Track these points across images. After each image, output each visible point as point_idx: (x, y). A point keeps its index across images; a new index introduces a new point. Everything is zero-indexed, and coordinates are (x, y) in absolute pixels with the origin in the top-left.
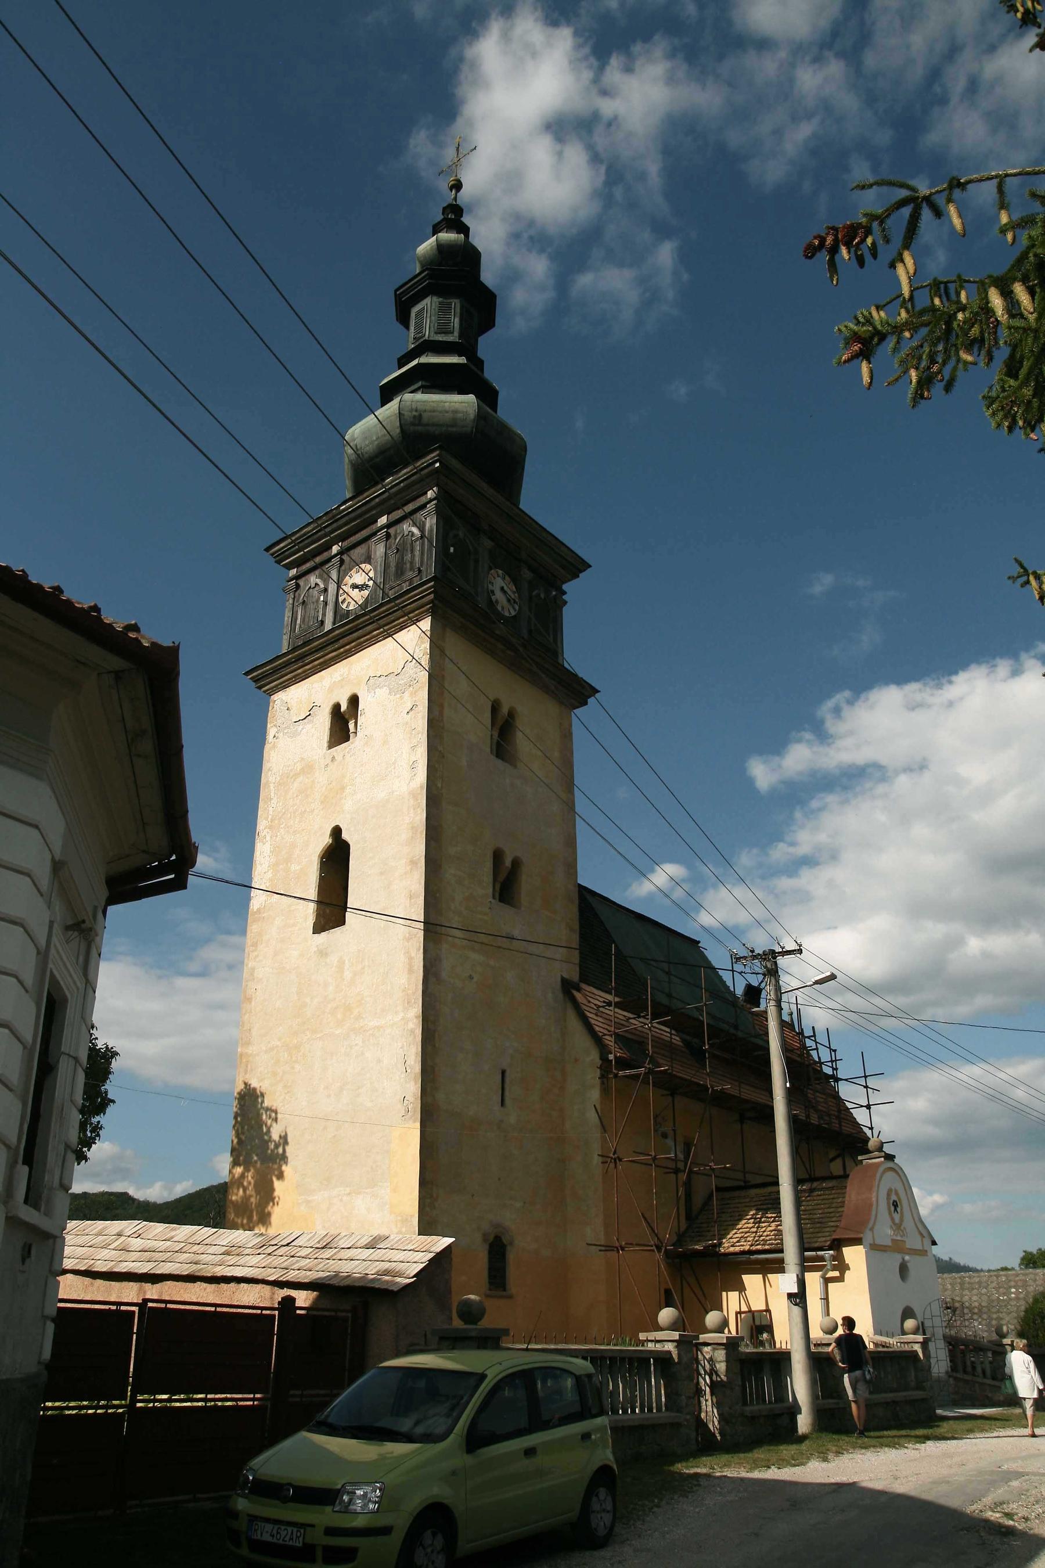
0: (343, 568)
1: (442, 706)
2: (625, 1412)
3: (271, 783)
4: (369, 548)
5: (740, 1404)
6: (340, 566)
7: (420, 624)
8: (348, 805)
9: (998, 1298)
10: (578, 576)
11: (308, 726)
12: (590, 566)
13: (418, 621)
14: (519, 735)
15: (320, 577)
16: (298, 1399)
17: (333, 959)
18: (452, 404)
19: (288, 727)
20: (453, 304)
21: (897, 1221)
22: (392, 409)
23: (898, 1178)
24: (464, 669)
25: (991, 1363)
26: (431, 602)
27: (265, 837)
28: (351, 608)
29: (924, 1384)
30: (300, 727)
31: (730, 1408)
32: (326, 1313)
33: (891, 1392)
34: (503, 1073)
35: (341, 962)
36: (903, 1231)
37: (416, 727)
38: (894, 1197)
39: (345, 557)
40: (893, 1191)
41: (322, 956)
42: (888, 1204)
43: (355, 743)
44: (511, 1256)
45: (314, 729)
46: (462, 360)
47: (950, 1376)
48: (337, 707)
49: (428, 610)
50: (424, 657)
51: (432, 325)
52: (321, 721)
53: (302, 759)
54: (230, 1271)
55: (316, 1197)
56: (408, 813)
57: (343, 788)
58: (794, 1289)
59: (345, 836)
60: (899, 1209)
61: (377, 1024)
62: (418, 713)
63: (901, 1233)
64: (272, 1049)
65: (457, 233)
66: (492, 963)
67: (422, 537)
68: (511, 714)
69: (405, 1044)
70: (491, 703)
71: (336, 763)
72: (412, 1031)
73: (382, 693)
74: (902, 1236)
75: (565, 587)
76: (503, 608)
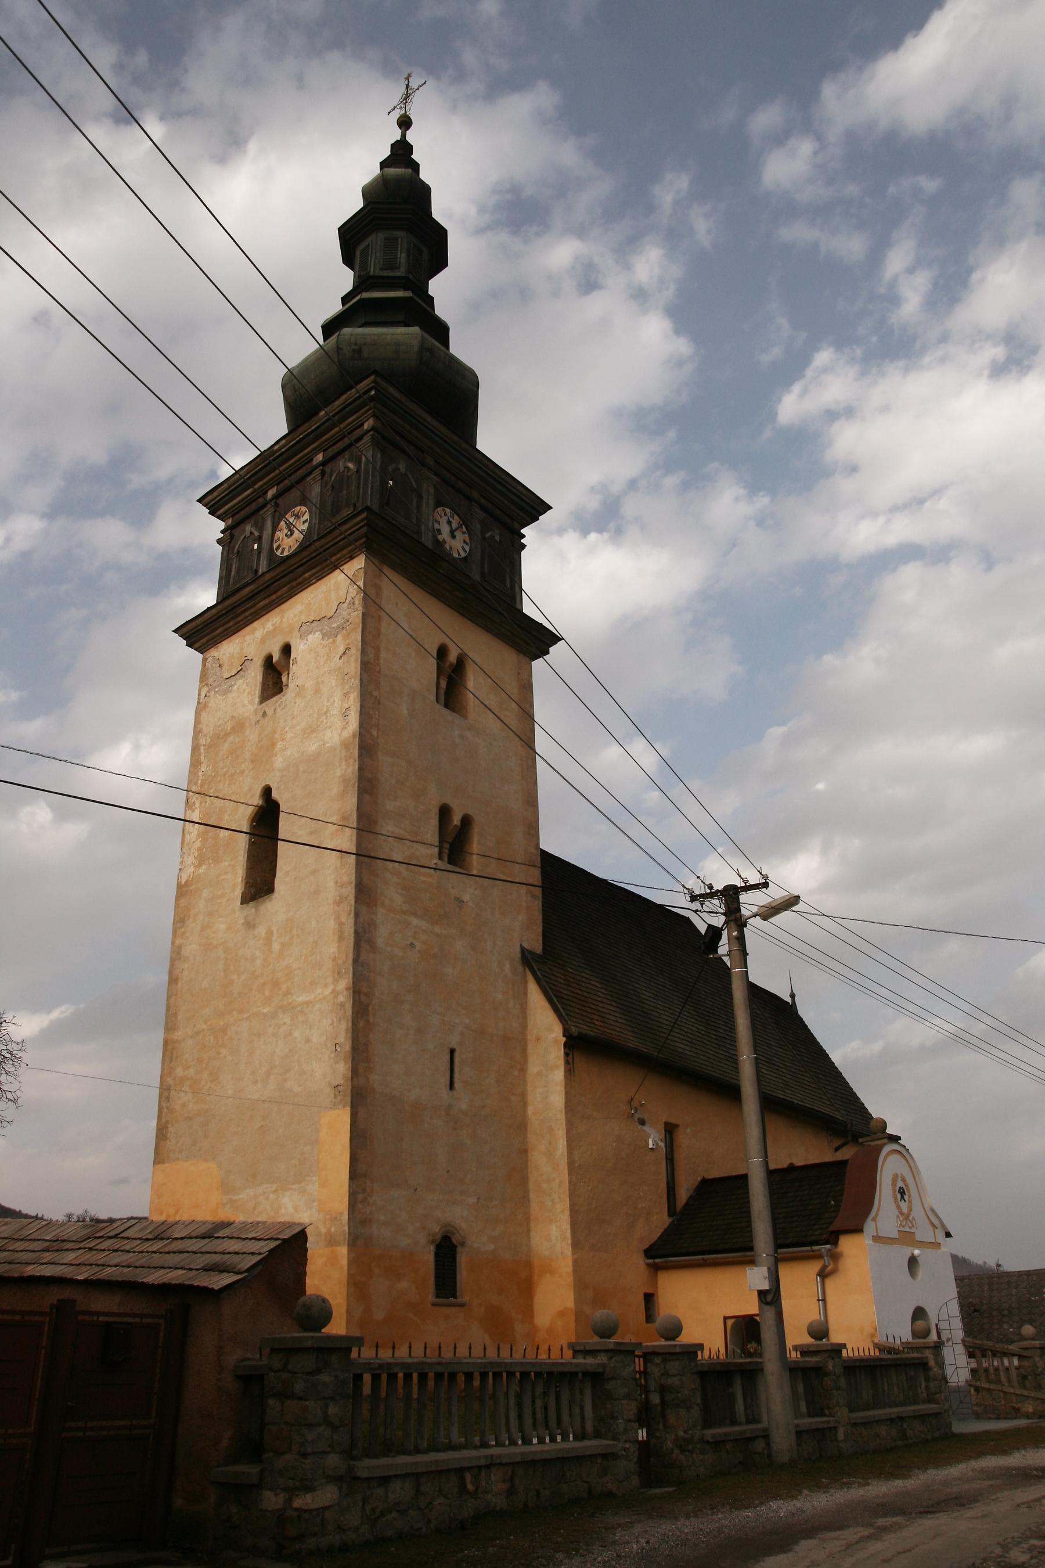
1: (377, 649)
2: (541, 1441)
5: (699, 1428)
8: (279, 762)
9: (1029, 1298)
10: (538, 519)
11: (240, 682)
12: (551, 508)
15: (256, 525)
16: (80, 1434)
17: (261, 930)
18: (395, 336)
19: (220, 685)
20: (400, 240)
21: (905, 1210)
22: (330, 344)
23: (904, 1162)
25: (1017, 1368)
26: (365, 535)
27: (194, 803)
28: (286, 554)
29: (938, 1396)
30: (232, 681)
31: (685, 1432)
32: (130, 1320)
33: (896, 1406)
34: (452, 1052)
35: (270, 933)
36: (911, 1223)
37: (349, 671)
38: (900, 1184)
40: (900, 1178)
41: (249, 928)
42: (894, 1191)
43: (289, 694)
44: (463, 1259)
45: (245, 685)
46: (407, 294)
47: (970, 1385)
48: (269, 659)
52: (253, 675)
53: (233, 717)
54: (41, 1270)
55: (241, 1196)
56: (340, 766)
57: (273, 745)
58: (765, 1286)
59: (275, 795)
60: (906, 1197)
61: (306, 999)
62: (351, 656)
63: (910, 1225)
64: (198, 1033)
65: (405, 168)
66: (437, 929)
67: (358, 471)
69: (335, 1019)
71: (267, 718)
72: (342, 1005)
73: (314, 638)
74: (910, 1228)
75: (522, 531)
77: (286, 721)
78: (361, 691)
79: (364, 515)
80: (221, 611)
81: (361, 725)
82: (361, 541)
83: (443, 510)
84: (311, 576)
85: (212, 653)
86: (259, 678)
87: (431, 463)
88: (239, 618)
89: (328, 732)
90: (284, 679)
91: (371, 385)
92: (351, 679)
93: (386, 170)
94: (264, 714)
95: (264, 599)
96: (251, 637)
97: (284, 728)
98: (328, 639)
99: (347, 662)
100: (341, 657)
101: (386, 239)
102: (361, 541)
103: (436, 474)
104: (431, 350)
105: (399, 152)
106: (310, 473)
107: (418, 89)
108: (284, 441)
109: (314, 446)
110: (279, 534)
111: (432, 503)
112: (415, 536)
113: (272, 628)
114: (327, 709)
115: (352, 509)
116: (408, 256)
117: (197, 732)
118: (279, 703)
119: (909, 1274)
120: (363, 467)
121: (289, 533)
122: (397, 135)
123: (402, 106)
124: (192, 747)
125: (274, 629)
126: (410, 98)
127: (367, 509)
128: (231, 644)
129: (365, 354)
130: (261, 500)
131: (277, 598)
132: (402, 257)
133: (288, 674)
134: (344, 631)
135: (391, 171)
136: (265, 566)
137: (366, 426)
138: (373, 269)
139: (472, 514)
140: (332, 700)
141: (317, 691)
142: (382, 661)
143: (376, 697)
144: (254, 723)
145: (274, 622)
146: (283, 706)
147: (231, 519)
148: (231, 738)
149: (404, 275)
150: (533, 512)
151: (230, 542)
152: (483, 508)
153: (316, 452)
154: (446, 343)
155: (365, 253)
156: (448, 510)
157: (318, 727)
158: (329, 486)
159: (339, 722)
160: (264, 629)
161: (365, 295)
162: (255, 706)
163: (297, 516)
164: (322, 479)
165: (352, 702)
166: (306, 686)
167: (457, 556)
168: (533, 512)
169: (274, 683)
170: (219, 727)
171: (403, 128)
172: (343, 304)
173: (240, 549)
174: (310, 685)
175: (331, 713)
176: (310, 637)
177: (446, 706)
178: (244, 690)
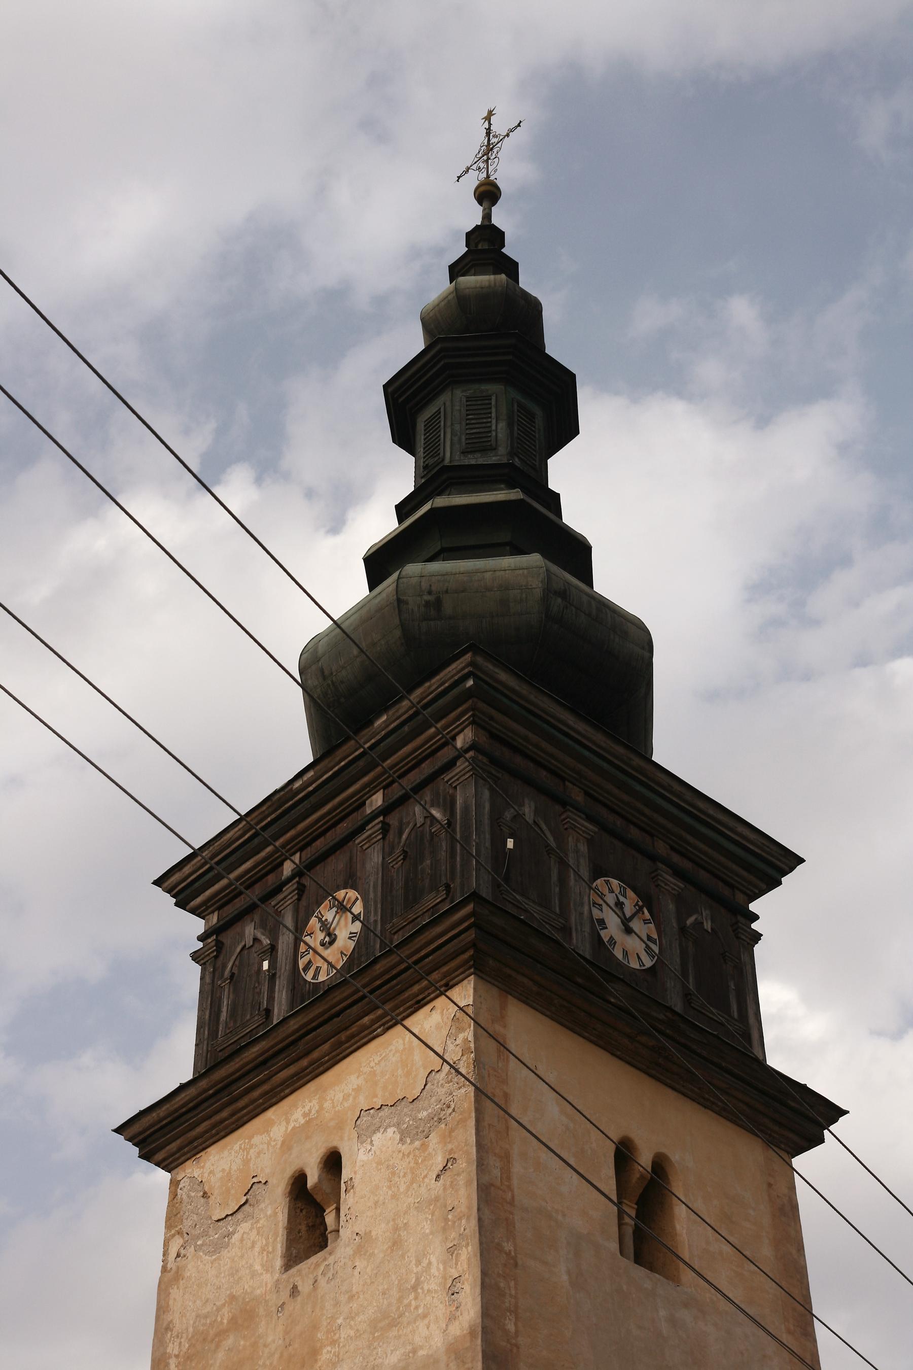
0: (304, 903)
1: (506, 1158)
3: (170, 1357)
4: (351, 859)
6: (299, 899)
7: (454, 993)
11: (245, 1226)
12: (801, 861)
13: (449, 986)
14: (680, 1212)
15: (263, 925)
18: (498, 573)
19: (205, 1234)
20: (494, 398)
22: (384, 595)
24: (551, 1078)
26: (473, 945)
28: (322, 978)
39: (306, 881)
45: (255, 1232)
46: (515, 494)
48: (299, 1179)
49: (467, 961)
50: (465, 1058)
51: (456, 439)
52: (269, 1212)
53: (232, 1298)
57: (314, 1353)
62: (458, 1174)
65: (494, 274)
67: (449, 824)
68: (660, 1166)
70: (612, 1148)
71: (299, 1298)
75: (753, 907)
76: (626, 953)
77: (337, 1304)
78: (481, 1243)
79: (470, 908)
80: (205, 1091)
81: (485, 1312)
82: (466, 956)
83: (607, 882)
84: (373, 1022)
85: (188, 1171)
86: (282, 1218)
87: (578, 796)
88: (241, 1103)
89: (421, 1325)
90: (330, 1219)
91: (466, 671)
92: (460, 1219)
94: (294, 1291)
95: (287, 1066)
96: (265, 1137)
97: (333, 1318)
98: (412, 1142)
99: (451, 1185)
100: (438, 1176)
101: (468, 399)
102: (466, 956)
103: (589, 818)
104: (564, 594)
105: (480, 247)
106: (361, 829)
107: (508, 135)
108: (311, 774)
109: (366, 779)
111: (585, 873)
112: (558, 936)
113: (302, 1121)
114: (417, 1279)
115: (443, 894)
116: (510, 425)
117: (162, 1330)
118: (322, 1268)
120: (458, 811)
121: (327, 939)
122: (473, 216)
123: (482, 165)
124: (153, 1361)
125: (308, 1123)
126: (495, 150)
127: (475, 896)
128: (226, 1153)
129: (448, 607)
130: (271, 878)
131: (311, 1064)
132: (500, 430)
133: (338, 1210)
134: (443, 1126)
135: (469, 281)
136: (284, 1002)
137: (459, 743)
138: (449, 455)
139: (657, 886)
140: (425, 1263)
141: (396, 1244)
142: (515, 1182)
143: (508, 1254)
144: (274, 1309)
145: (307, 1109)
146: (330, 1275)
147: (216, 914)
148: (229, 1342)
149: (505, 461)
150: (771, 871)
151: (216, 957)
152: (678, 873)
153: (370, 790)
154: (586, 575)
155: (433, 424)
156: (615, 882)
157: (400, 1316)
158: (398, 851)
159: (441, 1306)
160: (288, 1122)
161: (441, 501)
162: (277, 1276)
163: (342, 908)
164: (383, 838)
165: (465, 1266)
166: (374, 1233)
167: (637, 967)
168: (771, 871)
169: (308, 1225)
170: (206, 1317)
171: (485, 204)
172: (401, 519)
173: (235, 971)
174: (380, 1231)
175: (426, 1287)
176: (377, 1138)
177: (639, 1259)
178: (254, 1244)
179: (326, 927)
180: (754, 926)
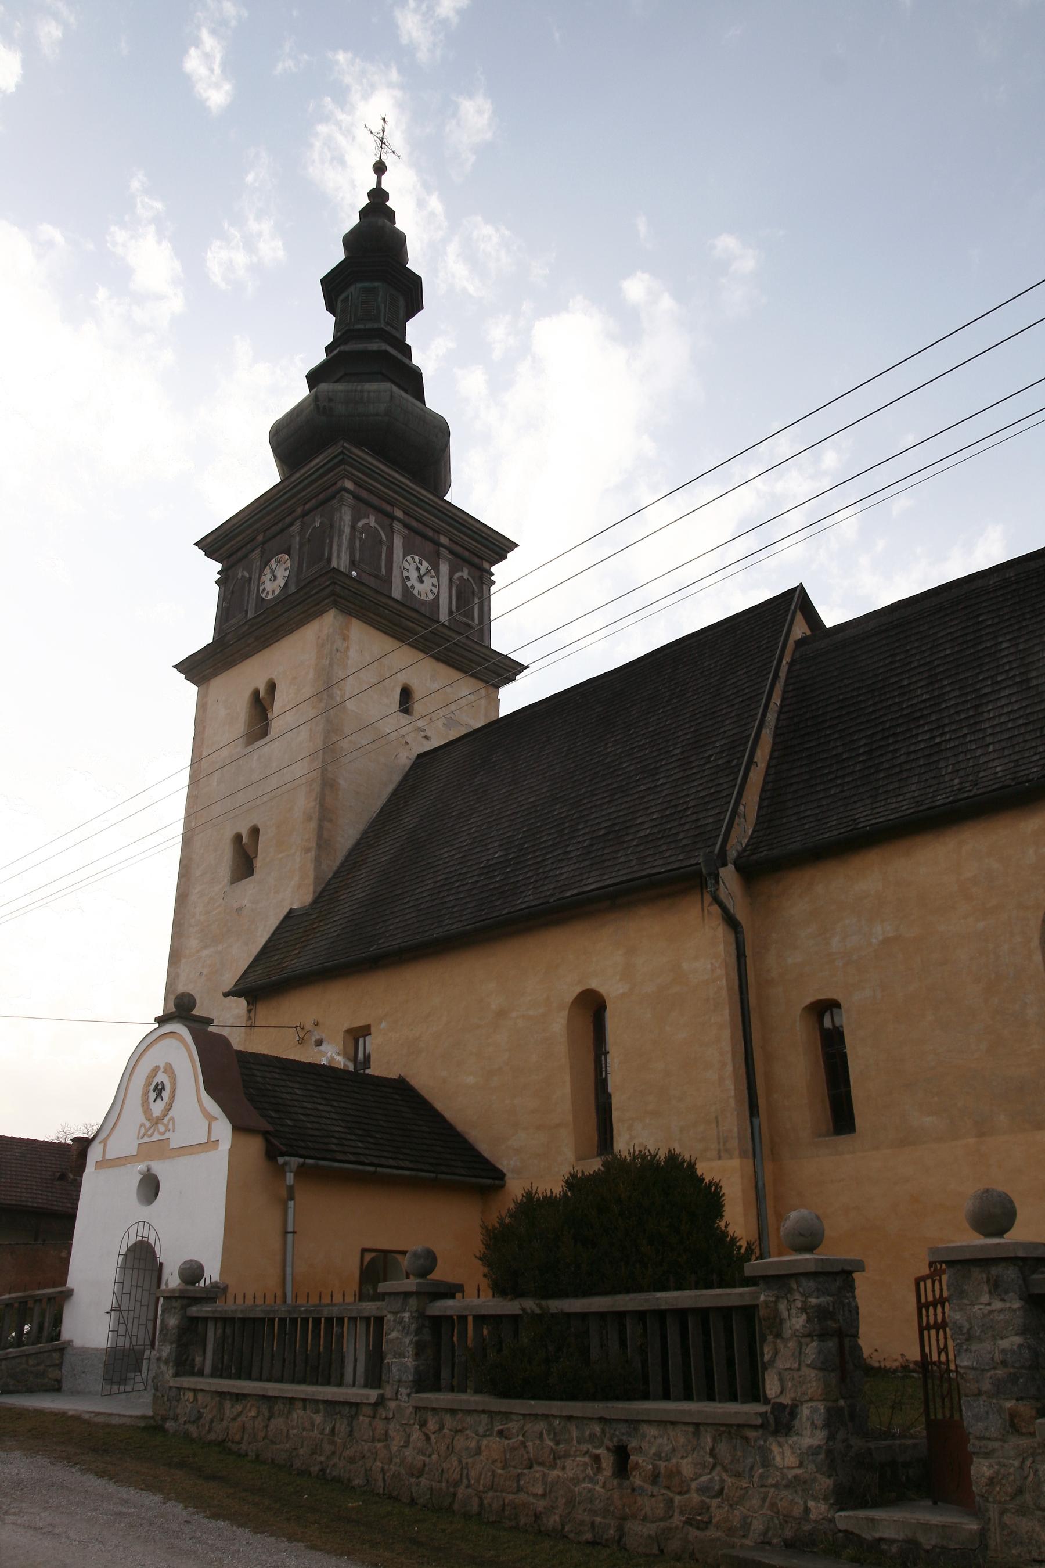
12: (517, 545)
48: (256, 693)
93: (323, 386)
110: (263, 578)
119: (434, 1272)
156: (416, 558)
161: (342, 348)
179: (272, 571)
180: (492, 578)
